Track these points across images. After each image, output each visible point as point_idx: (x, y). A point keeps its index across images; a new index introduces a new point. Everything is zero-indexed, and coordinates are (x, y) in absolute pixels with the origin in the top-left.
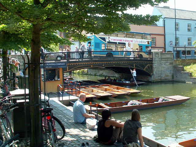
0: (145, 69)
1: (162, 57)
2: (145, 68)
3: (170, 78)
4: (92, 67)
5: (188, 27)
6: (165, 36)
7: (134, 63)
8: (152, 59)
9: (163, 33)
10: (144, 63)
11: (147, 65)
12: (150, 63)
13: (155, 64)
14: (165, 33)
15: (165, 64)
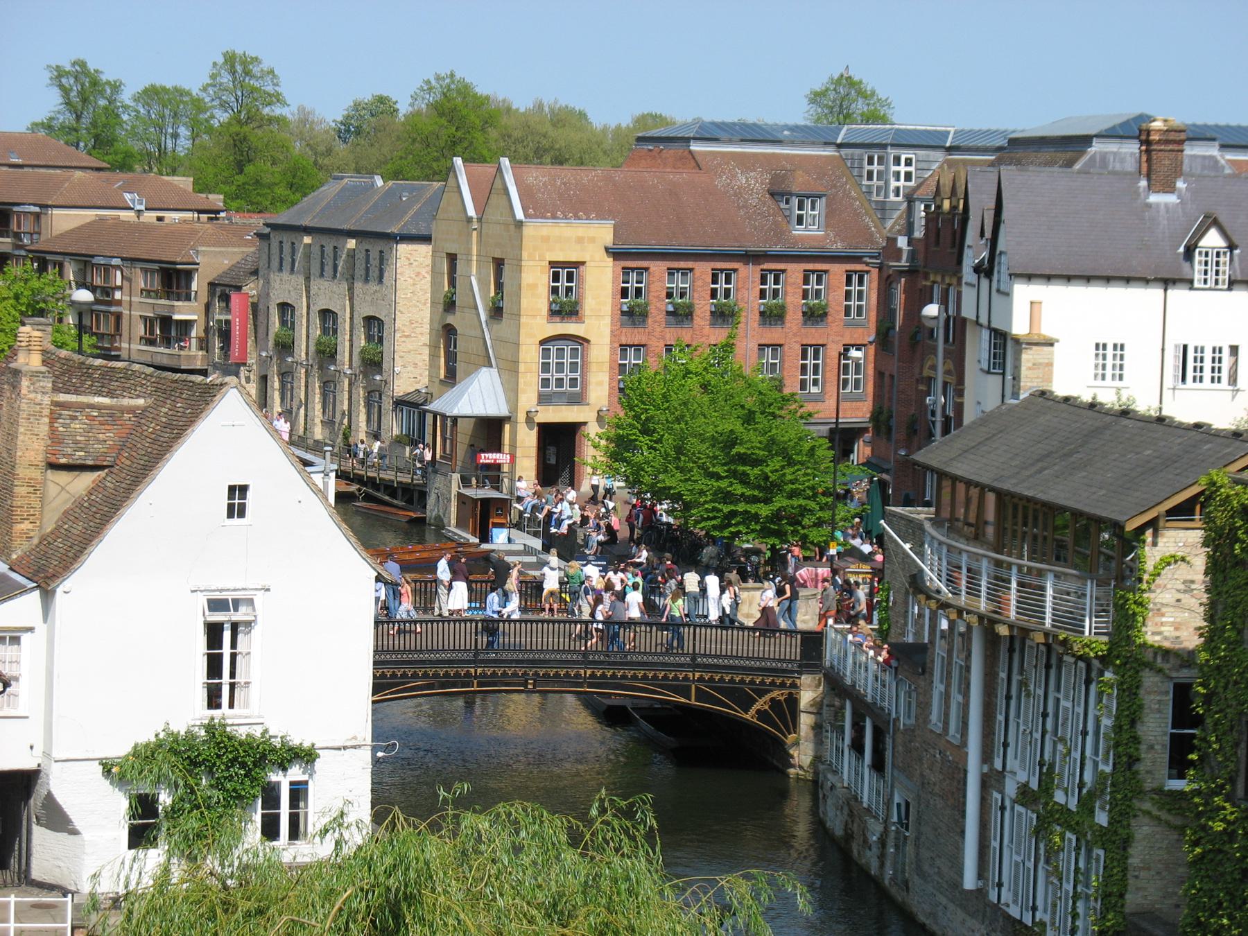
0: (753, 711)
2: (757, 706)
10: (752, 682)
11: (767, 697)
12: (783, 685)
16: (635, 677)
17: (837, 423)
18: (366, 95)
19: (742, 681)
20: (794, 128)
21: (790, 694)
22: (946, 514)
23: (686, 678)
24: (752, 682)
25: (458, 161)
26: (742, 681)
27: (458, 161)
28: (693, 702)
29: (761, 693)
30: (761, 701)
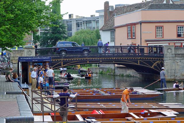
0: (153, 66)
1: (177, 53)
2: (154, 65)
4: (88, 63)
5: (81, 23)
7: (139, 60)
8: (163, 55)
10: (152, 59)
11: (156, 63)
12: (160, 60)
13: (167, 61)
15: (180, 62)
16: (125, 59)
17: (3, 96)
18: (108, 1)
19: (150, 59)
20: (111, 36)
21: (161, 62)
22: (44, 79)
23: (137, 59)
24: (152, 59)
25: (25, 83)
26: (150, 59)
27: (25, 83)
28: (139, 64)
29: (155, 62)
30: (155, 64)
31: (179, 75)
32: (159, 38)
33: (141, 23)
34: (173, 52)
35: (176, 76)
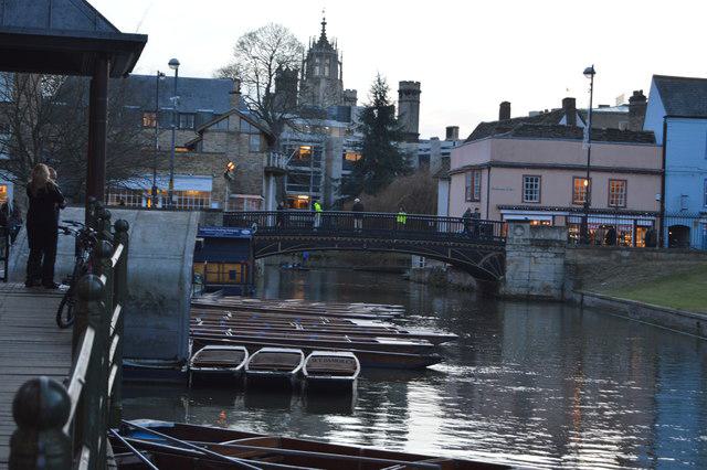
3: (554, 293)
6: (662, 174)
9: (657, 166)
14: (664, 167)
31: (537, 284)
32: (529, 203)
33: (489, 166)
34: (528, 235)
35: (532, 288)
